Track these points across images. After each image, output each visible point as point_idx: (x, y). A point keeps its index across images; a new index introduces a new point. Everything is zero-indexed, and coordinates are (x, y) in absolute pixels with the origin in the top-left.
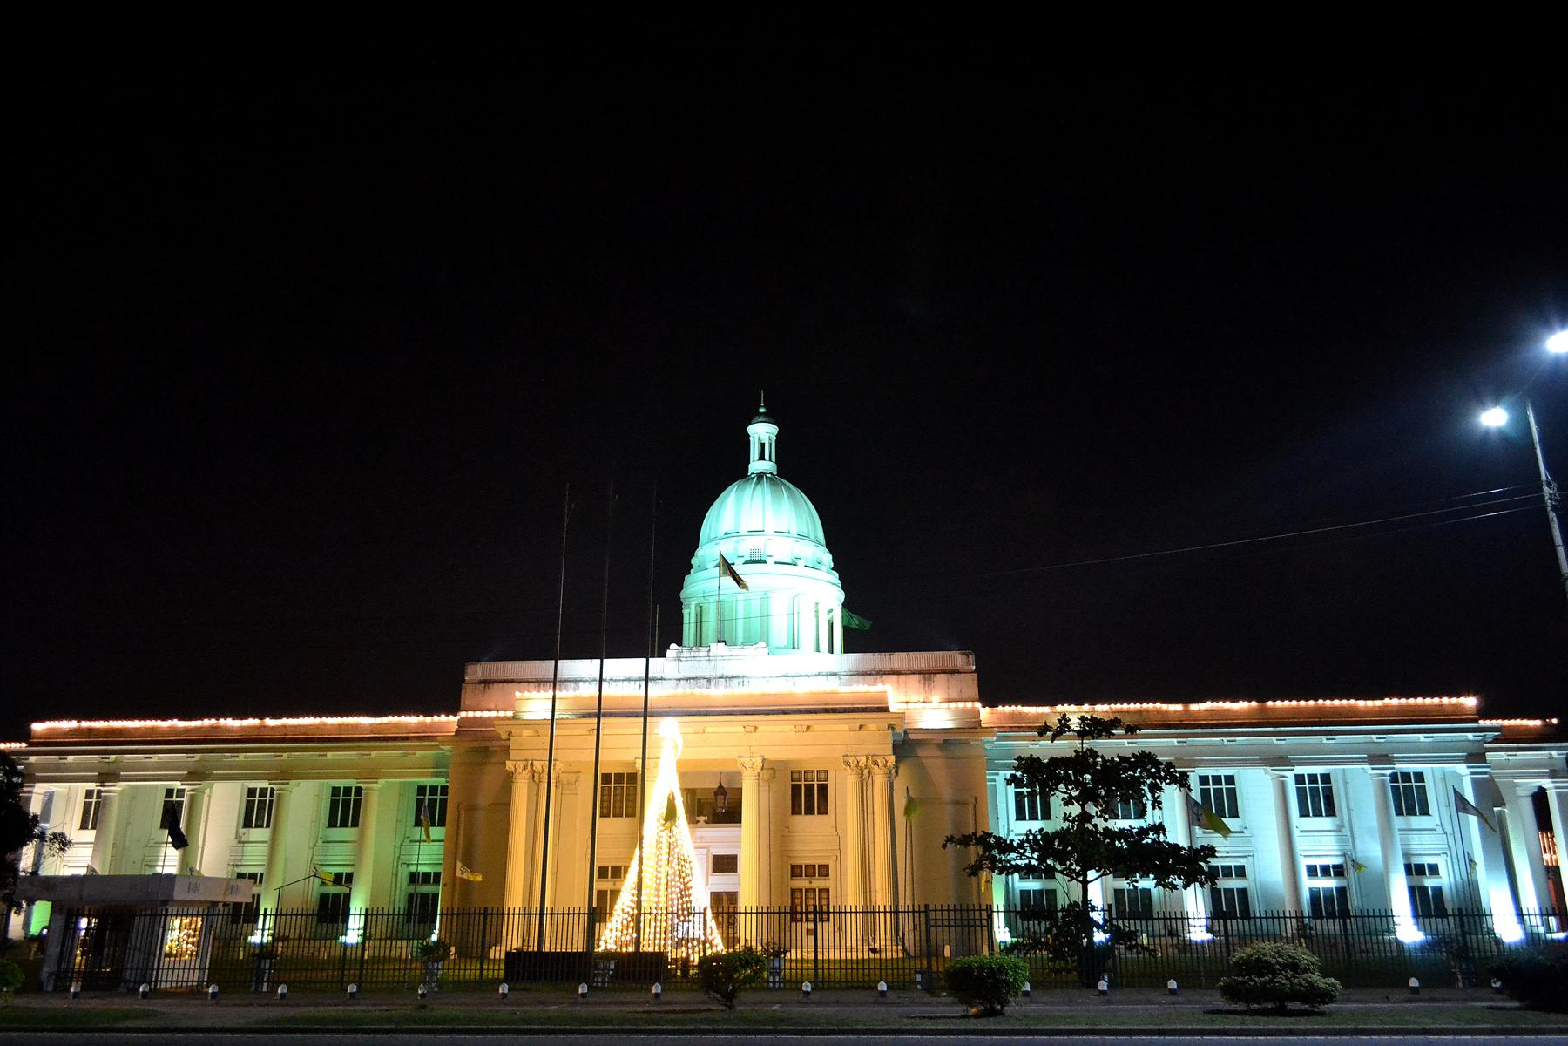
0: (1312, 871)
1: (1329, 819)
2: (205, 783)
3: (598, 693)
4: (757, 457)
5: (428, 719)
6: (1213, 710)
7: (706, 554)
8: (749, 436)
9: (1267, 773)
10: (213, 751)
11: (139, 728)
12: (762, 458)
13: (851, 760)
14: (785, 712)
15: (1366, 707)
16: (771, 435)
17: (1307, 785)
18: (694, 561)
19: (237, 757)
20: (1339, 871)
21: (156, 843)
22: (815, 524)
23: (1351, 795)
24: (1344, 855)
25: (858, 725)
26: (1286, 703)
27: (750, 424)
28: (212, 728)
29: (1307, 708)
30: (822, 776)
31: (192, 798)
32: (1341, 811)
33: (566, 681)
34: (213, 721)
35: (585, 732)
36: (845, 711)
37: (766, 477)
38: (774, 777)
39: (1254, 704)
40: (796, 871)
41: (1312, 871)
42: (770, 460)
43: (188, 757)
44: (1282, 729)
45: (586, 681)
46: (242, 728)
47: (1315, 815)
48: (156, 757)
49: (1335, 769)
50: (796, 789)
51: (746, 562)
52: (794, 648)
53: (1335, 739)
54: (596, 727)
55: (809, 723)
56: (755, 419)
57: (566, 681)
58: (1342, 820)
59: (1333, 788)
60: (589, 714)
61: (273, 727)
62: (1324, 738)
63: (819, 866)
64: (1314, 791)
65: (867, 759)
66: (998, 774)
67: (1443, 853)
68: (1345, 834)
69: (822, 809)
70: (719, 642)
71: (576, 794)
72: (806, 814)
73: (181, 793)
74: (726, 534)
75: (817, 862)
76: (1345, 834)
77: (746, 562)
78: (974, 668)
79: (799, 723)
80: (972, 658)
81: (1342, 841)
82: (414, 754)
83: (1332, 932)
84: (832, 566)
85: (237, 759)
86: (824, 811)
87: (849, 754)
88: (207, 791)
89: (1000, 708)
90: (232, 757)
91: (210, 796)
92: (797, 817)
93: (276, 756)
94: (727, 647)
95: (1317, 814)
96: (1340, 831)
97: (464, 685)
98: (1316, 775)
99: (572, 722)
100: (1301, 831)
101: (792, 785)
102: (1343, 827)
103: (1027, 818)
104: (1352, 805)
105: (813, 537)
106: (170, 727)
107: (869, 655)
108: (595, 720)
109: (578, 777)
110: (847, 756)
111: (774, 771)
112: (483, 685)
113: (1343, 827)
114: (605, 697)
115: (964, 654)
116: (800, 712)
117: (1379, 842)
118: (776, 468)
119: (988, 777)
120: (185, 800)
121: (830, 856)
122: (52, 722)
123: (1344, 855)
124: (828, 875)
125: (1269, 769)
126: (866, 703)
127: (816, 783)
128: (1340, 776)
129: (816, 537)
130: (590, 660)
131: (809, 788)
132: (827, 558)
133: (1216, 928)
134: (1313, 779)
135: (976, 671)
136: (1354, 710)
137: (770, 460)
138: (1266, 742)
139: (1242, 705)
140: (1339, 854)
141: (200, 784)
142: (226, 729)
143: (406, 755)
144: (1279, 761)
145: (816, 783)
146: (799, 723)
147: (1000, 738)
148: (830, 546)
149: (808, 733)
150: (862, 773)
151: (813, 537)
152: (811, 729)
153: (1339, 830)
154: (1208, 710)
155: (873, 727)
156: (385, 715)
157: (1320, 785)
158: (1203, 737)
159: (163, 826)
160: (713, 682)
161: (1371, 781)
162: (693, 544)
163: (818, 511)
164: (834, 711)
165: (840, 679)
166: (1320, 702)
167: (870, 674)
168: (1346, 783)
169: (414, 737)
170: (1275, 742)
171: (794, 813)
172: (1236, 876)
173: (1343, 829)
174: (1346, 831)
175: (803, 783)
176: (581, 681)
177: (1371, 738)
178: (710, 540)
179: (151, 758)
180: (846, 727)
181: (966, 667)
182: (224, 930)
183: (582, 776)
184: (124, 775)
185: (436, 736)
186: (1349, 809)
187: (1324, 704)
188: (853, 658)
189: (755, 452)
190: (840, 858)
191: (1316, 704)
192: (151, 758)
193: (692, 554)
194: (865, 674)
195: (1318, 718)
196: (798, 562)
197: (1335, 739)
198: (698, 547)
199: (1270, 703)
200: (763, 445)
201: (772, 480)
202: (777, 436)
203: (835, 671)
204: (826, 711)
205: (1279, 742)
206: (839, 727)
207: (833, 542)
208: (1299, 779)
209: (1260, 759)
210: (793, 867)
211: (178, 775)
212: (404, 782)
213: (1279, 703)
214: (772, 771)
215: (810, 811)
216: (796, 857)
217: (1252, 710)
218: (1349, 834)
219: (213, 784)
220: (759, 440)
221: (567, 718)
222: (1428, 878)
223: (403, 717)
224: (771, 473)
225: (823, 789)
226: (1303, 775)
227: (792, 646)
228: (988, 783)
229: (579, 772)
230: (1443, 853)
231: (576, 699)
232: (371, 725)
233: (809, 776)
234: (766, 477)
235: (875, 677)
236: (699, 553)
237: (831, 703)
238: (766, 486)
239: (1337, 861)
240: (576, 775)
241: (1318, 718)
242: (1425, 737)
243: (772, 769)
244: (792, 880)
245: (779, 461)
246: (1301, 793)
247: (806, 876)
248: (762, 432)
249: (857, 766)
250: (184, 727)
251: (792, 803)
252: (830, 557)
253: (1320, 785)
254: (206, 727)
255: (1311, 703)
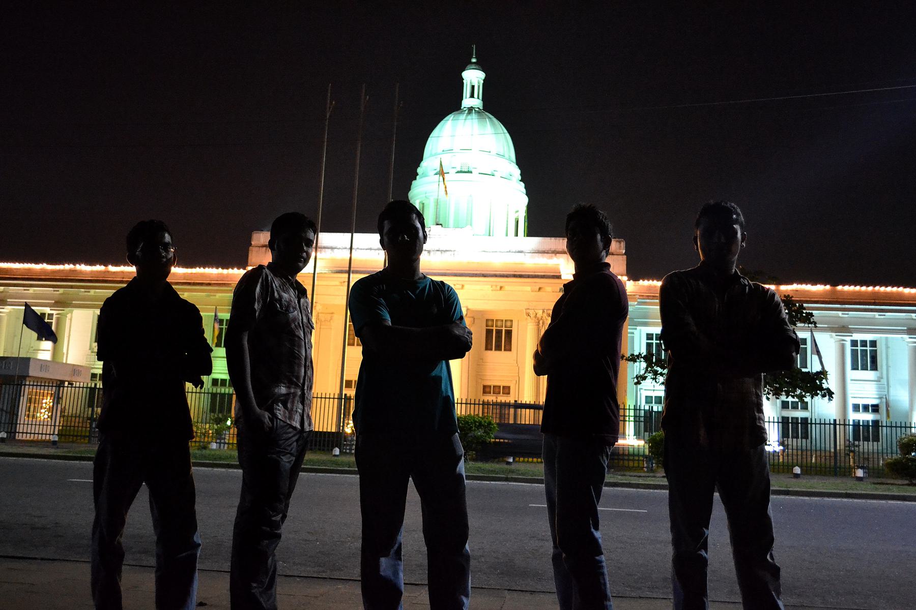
0: (856, 408)
1: (873, 372)
2: (67, 310)
3: (349, 255)
4: (469, 95)
5: (225, 271)
6: (797, 291)
7: (428, 165)
8: (463, 80)
9: (832, 337)
10: (72, 287)
11: (20, 269)
12: (472, 96)
13: (531, 312)
14: (484, 276)
15: (910, 293)
16: (480, 80)
17: (859, 348)
18: (419, 170)
19: (89, 292)
20: (875, 409)
21: (34, 350)
22: (509, 147)
23: (890, 357)
24: (880, 398)
25: (538, 288)
26: (852, 288)
27: (464, 70)
28: (71, 271)
29: (866, 292)
30: (509, 324)
31: (58, 319)
32: (882, 366)
33: (325, 248)
34: (71, 266)
35: (338, 283)
36: (529, 277)
37: (475, 110)
38: (474, 323)
39: (828, 287)
40: (486, 390)
41: (856, 408)
42: (478, 98)
43: (54, 291)
44: (847, 306)
45: (340, 248)
46: (92, 272)
47: (862, 369)
48: (32, 290)
49: (881, 337)
50: (489, 332)
51: (458, 172)
52: (490, 235)
53: (885, 315)
54: (347, 280)
55: (501, 284)
56: (469, 67)
57: (325, 248)
58: (882, 373)
59: (878, 351)
60: (342, 271)
61: (114, 272)
62: (876, 314)
63: (494, 386)
64: (864, 352)
65: (543, 312)
66: (636, 329)
67: (640, 391)
68: (884, 384)
69: (507, 348)
70: (437, 224)
71: (331, 329)
72: (495, 350)
73: (51, 316)
74: (443, 151)
75: (502, 384)
76: (884, 384)
77: (458, 172)
78: (624, 251)
79: (494, 284)
80: (623, 244)
81: (880, 388)
82: (215, 296)
83: (866, 450)
84: (520, 178)
85: (89, 294)
86: (508, 348)
87: (530, 308)
88: (69, 316)
89: (641, 282)
90: (85, 292)
91: (71, 320)
92: (489, 352)
93: (25, 290)
94: (442, 228)
95: (864, 368)
96: (879, 381)
97: (251, 248)
98: (867, 341)
99: (326, 275)
100: (852, 380)
101: (487, 329)
102: (882, 378)
103: (860, 369)
104: (890, 363)
105: (507, 156)
106: (41, 269)
107: (547, 239)
108: (347, 275)
109: (332, 317)
110: (528, 309)
111: (474, 319)
112: (265, 248)
113: (882, 378)
114: (354, 260)
115: (617, 241)
116: (496, 276)
117: (908, 389)
118: (482, 105)
119: (629, 331)
120: (54, 321)
121: (511, 381)
122: (9, 264)
123: (880, 398)
124: (509, 394)
125: (834, 334)
126: (545, 272)
127: (504, 329)
128: (884, 342)
129: (509, 156)
130: (549, 238)
131: (499, 332)
132: (517, 172)
133: (786, 443)
134: (864, 343)
135: (625, 254)
136: (900, 295)
137: (478, 98)
138: (834, 315)
139: (819, 288)
140: (877, 397)
141: (63, 310)
142: (81, 272)
143: (208, 296)
144: (842, 329)
145: (504, 329)
146: (494, 284)
147: (640, 303)
148: (519, 163)
149: (501, 292)
150: (539, 322)
151: (507, 156)
152: (502, 289)
153: (878, 380)
154: (793, 290)
155: (549, 289)
156: (791, 283)
157: (868, 348)
158: (14, 286)
159: (96, 342)
160: (432, 253)
161: (907, 347)
162: (419, 158)
163: (511, 136)
164: (521, 276)
165: (525, 255)
166: (877, 288)
167: (548, 253)
168: (887, 347)
169: (215, 284)
170: (841, 315)
171: (487, 349)
172: (801, 409)
173: (882, 380)
174: (884, 381)
175: (494, 328)
176: (335, 248)
177: (911, 316)
178: (432, 155)
179: (28, 290)
180: (529, 288)
181: (618, 251)
182: (82, 411)
183: (335, 316)
184: (9, 302)
185: (230, 284)
186: (888, 367)
187: (860, 290)
188: (535, 242)
189: (467, 91)
190: (518, 382)
191: (873, 290)
192: (28, 290)
193: (418, 165)
194: (544, 252)
195: (875, 300)
196: (495, 173)
197: (885, 315)
198: (422, 160)
199: (840, 288)
200: (473, 87)
201: (479, 113)
202: (484, 80)
203: (522, 250)
204: (515, 276)
205: (843, 316)
206: (525, 288)
207: (521, 161)
208: (854, 343)
209: (828, 327)
210: (484, 387)
211: (48, 303)
212: (208, 316)
213: (846, 288)
214: (472, 319)
215: (498, 348)
216: (487, 380)
217: (826, 292)
218: (886, 383)
219: (72, 311)
220: (471, 83)
221: (325, 273)
222: (791, 411)
223: (207, 268)
224: (478, 108)
225: (509, 333)
226: (857, 341)
227: (488, 234)
228: (629, 335)
229: (332, 313)
230: (640, 391)
231: (333, 260)
232: (184, 274)
233: (499, 323)
234: (475, 110)
235: (551, 254)
236: (423, 164)
237: (519, 270)
238: (474, 116)
239: (875, 402)
240: (330, 315)
241: (875, 300)
242: (842, 314)
243: (473, 317)
244: (483, 395)
245: (485, 99)
246: (854, 353)
247: (493, 393)
248: (473, 77)
249: (536, 316)
250: (51, 270)
251: (486, 342)
252: (519, 172)
253: (868, 348)
254: (67, 270)
255: (870, 288)
